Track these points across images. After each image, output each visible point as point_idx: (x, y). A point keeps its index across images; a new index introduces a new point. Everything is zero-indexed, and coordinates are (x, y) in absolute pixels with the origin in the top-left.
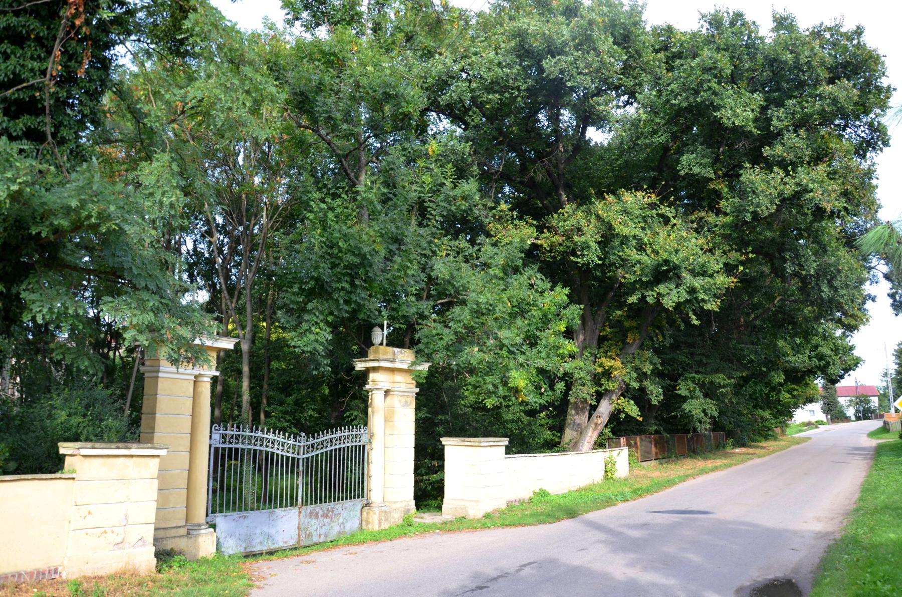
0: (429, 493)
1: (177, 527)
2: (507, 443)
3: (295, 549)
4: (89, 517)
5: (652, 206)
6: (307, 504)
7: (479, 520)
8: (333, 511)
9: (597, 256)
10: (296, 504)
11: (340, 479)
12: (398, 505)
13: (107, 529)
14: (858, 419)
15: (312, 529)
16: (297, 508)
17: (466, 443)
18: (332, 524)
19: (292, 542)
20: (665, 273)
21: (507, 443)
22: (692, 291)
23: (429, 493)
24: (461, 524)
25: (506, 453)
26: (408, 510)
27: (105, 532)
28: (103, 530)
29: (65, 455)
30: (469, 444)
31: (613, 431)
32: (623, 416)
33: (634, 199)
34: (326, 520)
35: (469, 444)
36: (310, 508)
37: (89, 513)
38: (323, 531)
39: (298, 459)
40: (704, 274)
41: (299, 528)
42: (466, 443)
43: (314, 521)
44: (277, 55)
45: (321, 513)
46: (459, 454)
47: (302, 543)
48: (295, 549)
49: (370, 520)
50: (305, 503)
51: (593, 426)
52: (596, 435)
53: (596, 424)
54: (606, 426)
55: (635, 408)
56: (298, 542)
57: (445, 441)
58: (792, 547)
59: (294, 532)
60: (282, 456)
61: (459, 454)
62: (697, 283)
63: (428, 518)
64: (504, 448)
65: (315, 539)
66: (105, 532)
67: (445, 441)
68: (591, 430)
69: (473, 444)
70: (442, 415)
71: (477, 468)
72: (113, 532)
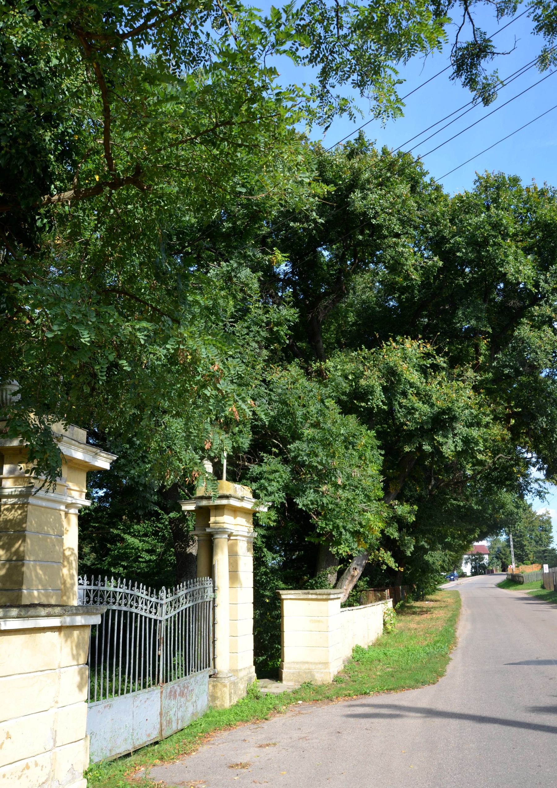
3: (157, 743)
5: (428, 355)
7: (329, 686)
9: (382, 401)
11: (191, 646)
13: (31, 761)
14: (474, 574)
17: (310, 596)
19: (155, 735)
20: (442, 421)
22: (467, 441)
24: (313, 693)
30: (314, 597)
31: (370, 584)
32: (385, 567)
33: (413, 347)
35: (314, 597)
38: (180, 714)
40: (479, 424)
41: (161, 714)
42: (310, 596)
46: (298, 610)
47: (166, 734)
48: (157, 743)
49: (219, 694)
51: (350, 578)
52: (351, 586)
53: (353, 576)
54: (360, 579)
55: (392, 560)
57: (285, 594)
59: (155, 719)
61: (298, 610)
62: (475, 433)
67: (285, 594)
68: (347, 582)
69: (319, 597)
71: (328, 628)
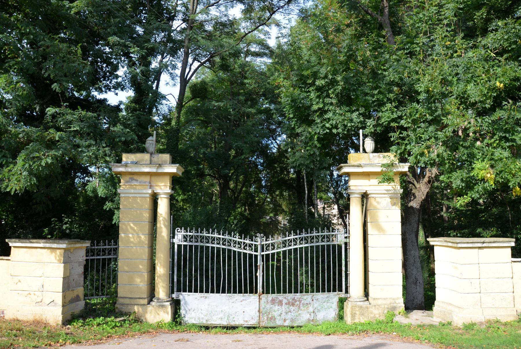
0: (420, 292)
1: (139, 298)
2: (513, 244)
4: (19, 283)
6: (268, 292)
8: (300, 301)
10: (256, 292)
12: (379, 302)
15: (276, 314)
16: (257, 295)
18: (300, 312)
21: (513, 244)
23: (420, 292)
25: (513, 256)
26: (394, 308)
27: (30, 294)
28: (28, 292)
29: (433, 246)
34: (292, 308)
36: (271, 296)
37: (20, 281)
39: (256, 256)
43: (277, 307)
44: (235, 19)
45: (285, 301)
47: (262, 324)
50: (267, 291)
56: (259, 323)
58: (240, 343)
60: (239, 253)
63: (418, 317)
64: (509, 250)
65: (279, 322)
66: (30, 294)
70: (428, 221)
72: (35, 295)
